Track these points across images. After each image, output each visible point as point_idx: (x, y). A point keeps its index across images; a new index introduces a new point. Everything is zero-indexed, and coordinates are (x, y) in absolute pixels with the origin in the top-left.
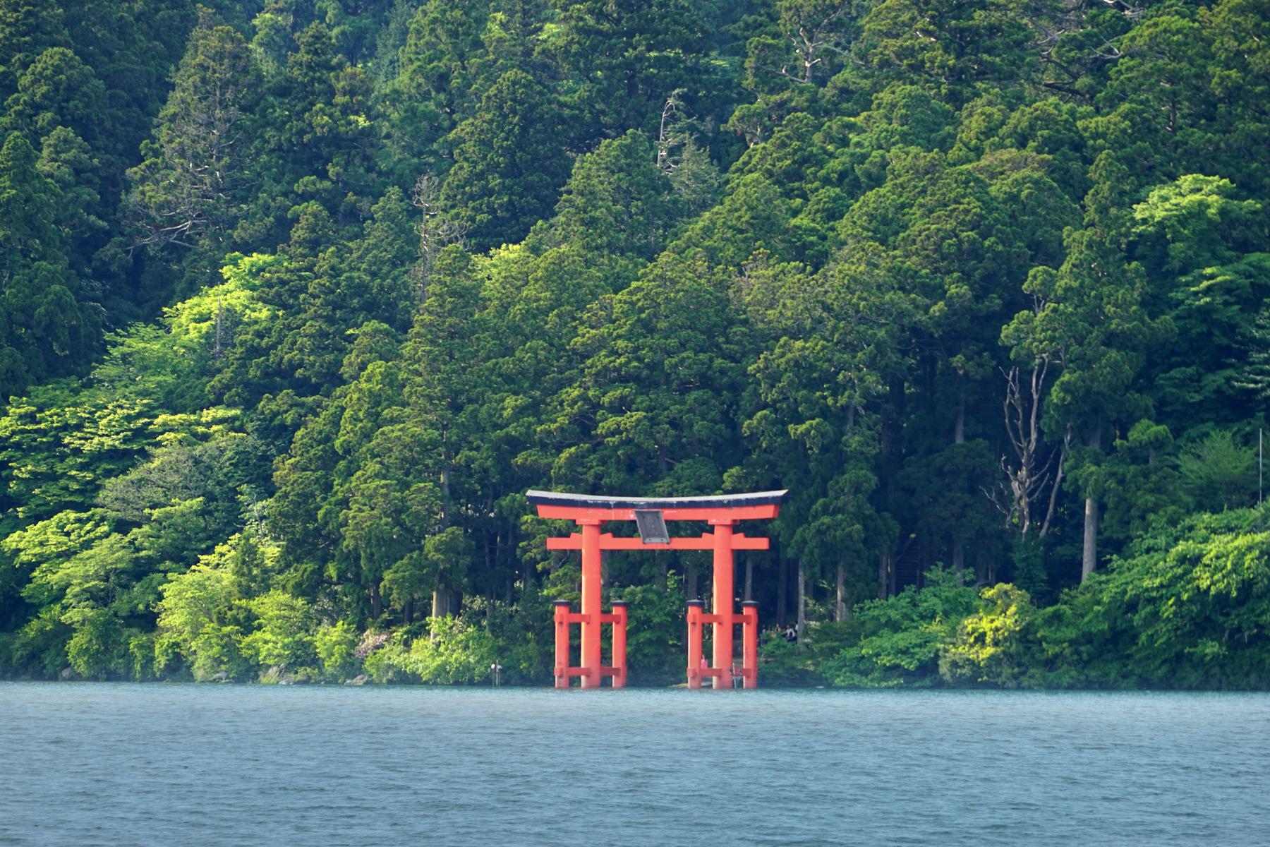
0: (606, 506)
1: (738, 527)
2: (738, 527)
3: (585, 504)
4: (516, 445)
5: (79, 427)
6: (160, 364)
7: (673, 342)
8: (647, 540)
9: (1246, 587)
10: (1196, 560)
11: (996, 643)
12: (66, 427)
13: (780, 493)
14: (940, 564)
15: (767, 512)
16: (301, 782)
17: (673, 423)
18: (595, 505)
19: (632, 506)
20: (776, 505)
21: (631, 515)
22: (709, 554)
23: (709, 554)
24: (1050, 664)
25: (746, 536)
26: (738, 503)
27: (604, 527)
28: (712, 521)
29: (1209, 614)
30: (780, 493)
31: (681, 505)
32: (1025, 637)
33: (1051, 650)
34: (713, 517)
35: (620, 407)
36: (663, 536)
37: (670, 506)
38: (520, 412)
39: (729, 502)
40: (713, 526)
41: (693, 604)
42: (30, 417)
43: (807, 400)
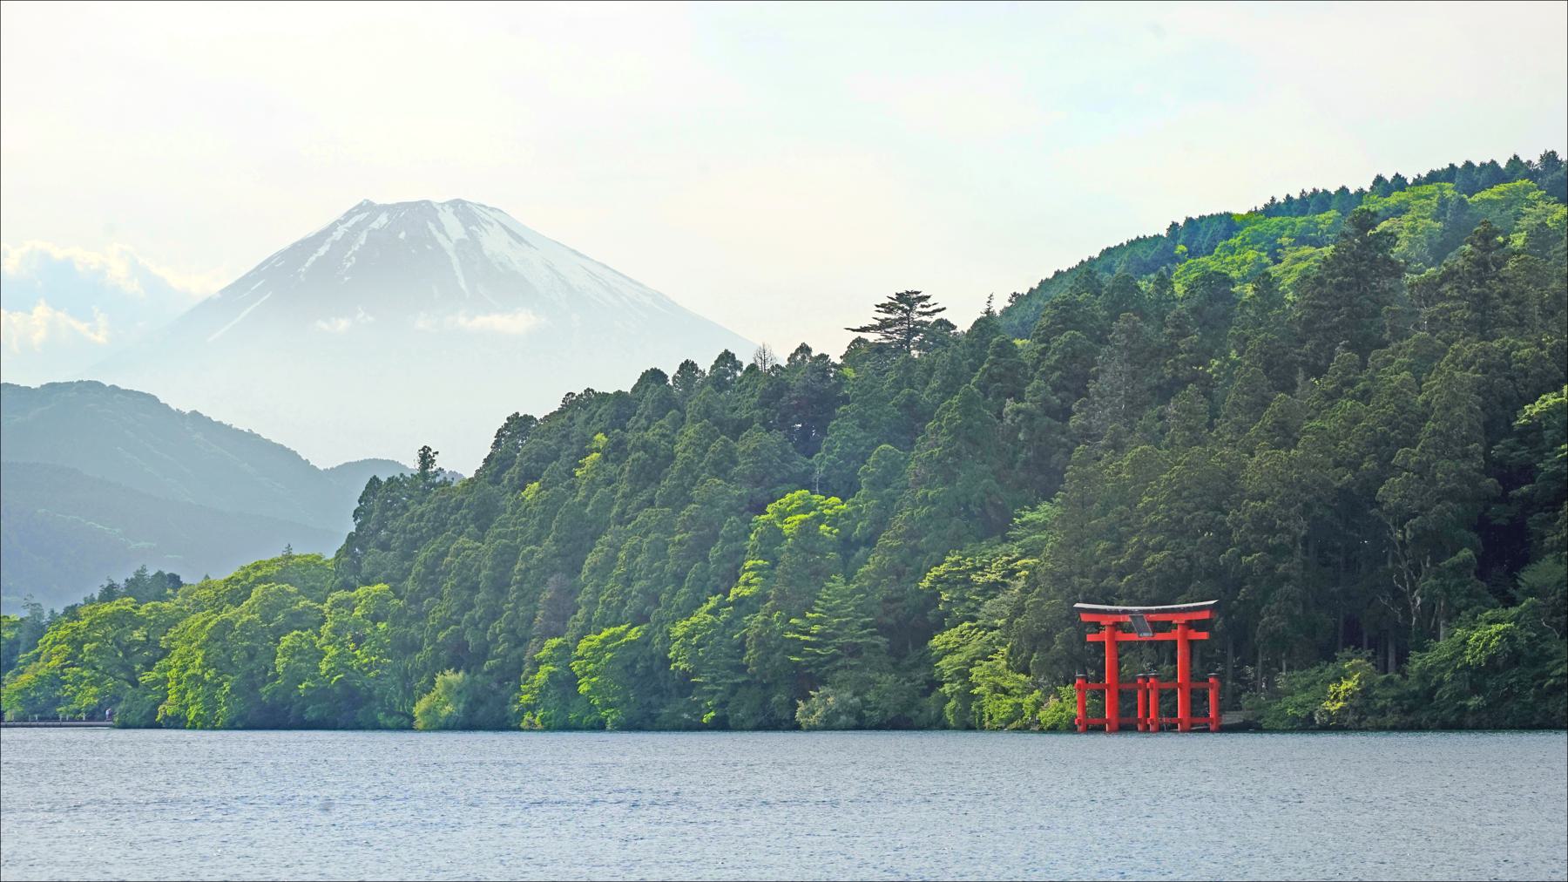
0: (1117, 612)
3: (1105, 611)
4: (1104, 573)
5: (982, 569)
7: (1190, 506)
9: (1491, 659)
10: (872, 682)
11: (1345, 699)
12: (975, 569)
15: (1206, 615)
17: (1188, 558)
18: (1111, 612)
24: (1383, 712)
26: (1189, 609)
29: (1477, 677)
32: (1365, 692)
33: (1381, 703)
35: (1159, 548)
38: (1108, 551)
42: (957, 563)
43: (1255, 541)
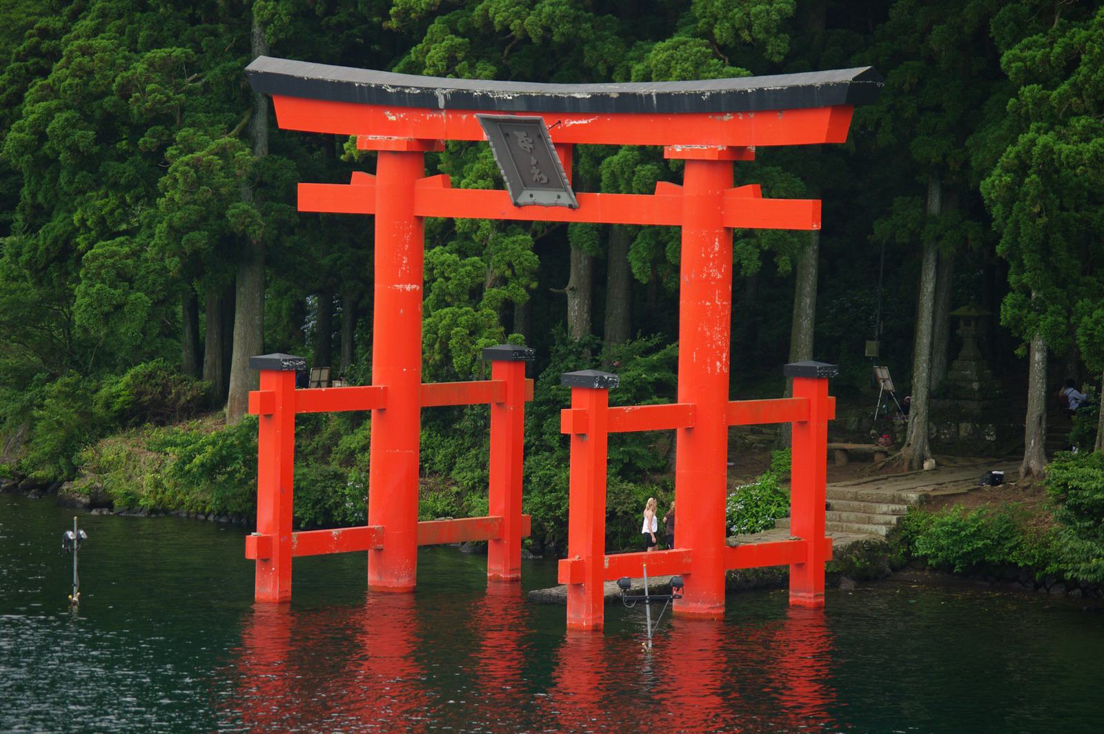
0: (426, 100)
1: (742, 167)
2: (742, 167)
6: (685, 24)
8: (524, 198)
13: (846, 75)
14: (356, 158)
15: (814, 129)
16: (795, 678)
19: (486, 103)
20: (836, 108)
21: (470, 126)
22: (663, 240)
23: (663, 240)
25: (768, 193)
27: (427, 158)
28: (676, 150)
30: (846, 75)
31: (598, 105)
34: (686, 143)
36: (559, 186)
37: (574, 107)
39: (716, 96)
40: (682, 165)
41: (586, 384)
